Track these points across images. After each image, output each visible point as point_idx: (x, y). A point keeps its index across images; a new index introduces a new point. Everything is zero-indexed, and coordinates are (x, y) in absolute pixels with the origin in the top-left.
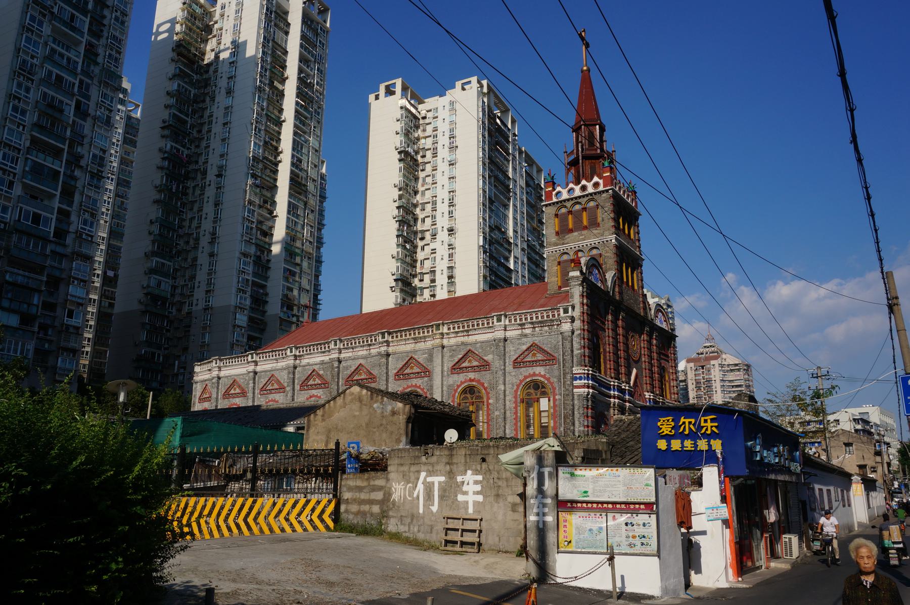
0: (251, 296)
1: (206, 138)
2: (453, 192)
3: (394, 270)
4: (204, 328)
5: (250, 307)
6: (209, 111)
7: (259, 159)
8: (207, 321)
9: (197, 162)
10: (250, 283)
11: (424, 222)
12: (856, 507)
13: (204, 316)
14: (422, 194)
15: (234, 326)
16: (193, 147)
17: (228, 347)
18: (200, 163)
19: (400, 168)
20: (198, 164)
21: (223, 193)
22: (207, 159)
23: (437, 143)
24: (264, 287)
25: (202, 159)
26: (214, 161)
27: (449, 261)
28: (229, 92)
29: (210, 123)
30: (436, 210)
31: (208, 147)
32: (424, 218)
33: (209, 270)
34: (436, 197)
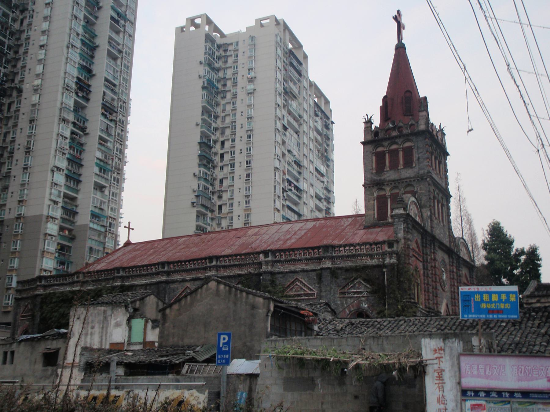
0: (62, 207)
1: (22, 59)
2: (251, 130)
3: (196, 188)
4: (23, 185)
5: (61, 218)
6: (26, 34)
7: (70, 110)
8: (19, 229)
9: (13, 81)
10: (62, 194)
11: (223, 169)
12: (537, 66)
13: (16, 225)
14: (223, 119)
15: (46, 234)
16: (9, 67)
17: (39, 254)
18: (16, 81)
19: (203, 95)
20: (14, 82)
21: (38, 110)
22: (28, 49)
23: (237, 73)
24: (73, 199)
25: (18, 79)
26: (21, 140)
27: (247, 167)
28: (28, 151)
29: (17, 118)
30: (235, 134)
31: (24, 67)
32: (222, 179)
33: (25, 165)
34: (235, 122)
